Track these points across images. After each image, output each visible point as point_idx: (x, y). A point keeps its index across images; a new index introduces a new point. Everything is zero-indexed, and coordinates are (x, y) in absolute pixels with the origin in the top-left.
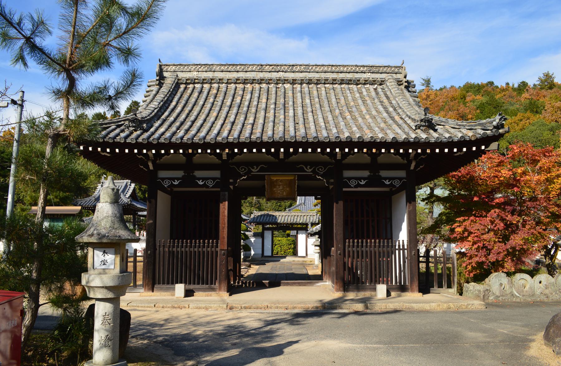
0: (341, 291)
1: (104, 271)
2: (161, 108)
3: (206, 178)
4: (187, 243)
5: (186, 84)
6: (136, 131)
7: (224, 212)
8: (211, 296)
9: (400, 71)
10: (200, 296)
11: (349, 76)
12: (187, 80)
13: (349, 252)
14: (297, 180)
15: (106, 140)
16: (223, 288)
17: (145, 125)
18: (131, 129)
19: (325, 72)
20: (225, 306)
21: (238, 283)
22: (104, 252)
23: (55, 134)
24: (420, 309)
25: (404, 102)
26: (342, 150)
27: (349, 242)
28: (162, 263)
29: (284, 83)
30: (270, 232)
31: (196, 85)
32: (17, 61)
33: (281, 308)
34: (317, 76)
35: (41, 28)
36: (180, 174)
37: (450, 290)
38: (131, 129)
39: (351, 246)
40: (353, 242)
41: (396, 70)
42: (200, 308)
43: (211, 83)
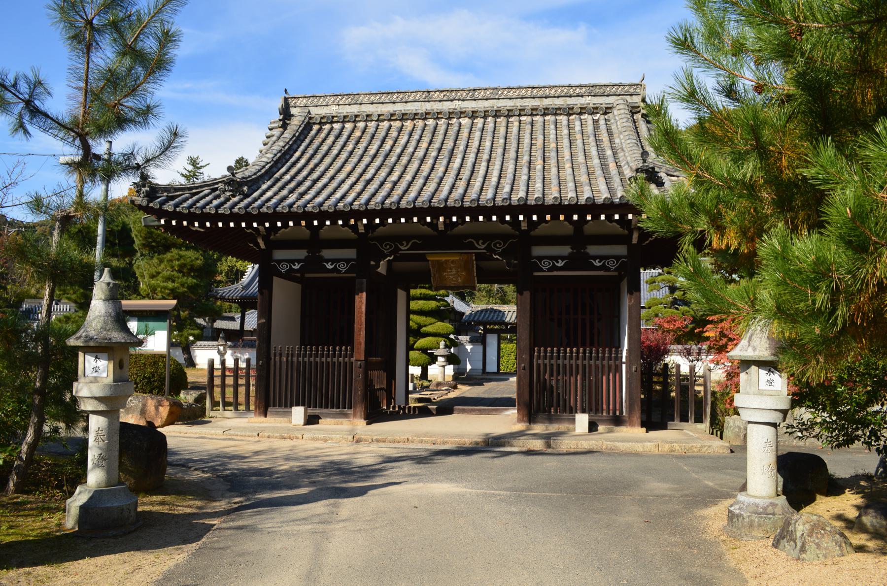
0: (525, 422)
1: (95, 380)
2: (276, 162)
3: (338, 260)
4: (311, 350)
5: (321, 123)
6: (234, 196)
7: (360, 308)
8: (342, 424)
9: (638, 90)
10: (328, 424)
11: (559, 102)
12: (322, 118)
13: (539, 365)
14: (476, 260)
15: (192, 210)
16: (358, 414)
17: (245, 188)
18: (228, 194)
19: (522, 98)
20: (350, 438)
21: (394, 408)
22: (96, 357)
23: (63, 217)
24: (628, 451)
25: (629, 141)
26: (528, 217)
27: (539, 352)
28: (278, 378)
29: (460, 117)
30: (495, 336)
31: (335, 125)
32: (16, 130)
33: (426, 442)
34: (509, 104)
35: (39, 90)
36: (302, 254)
37: (699, 426)
38: (228, 194)
39: (580, 358)
40: (546, 352)
41: (632, 90)
42: (317, 439)
43: (355, 121)
